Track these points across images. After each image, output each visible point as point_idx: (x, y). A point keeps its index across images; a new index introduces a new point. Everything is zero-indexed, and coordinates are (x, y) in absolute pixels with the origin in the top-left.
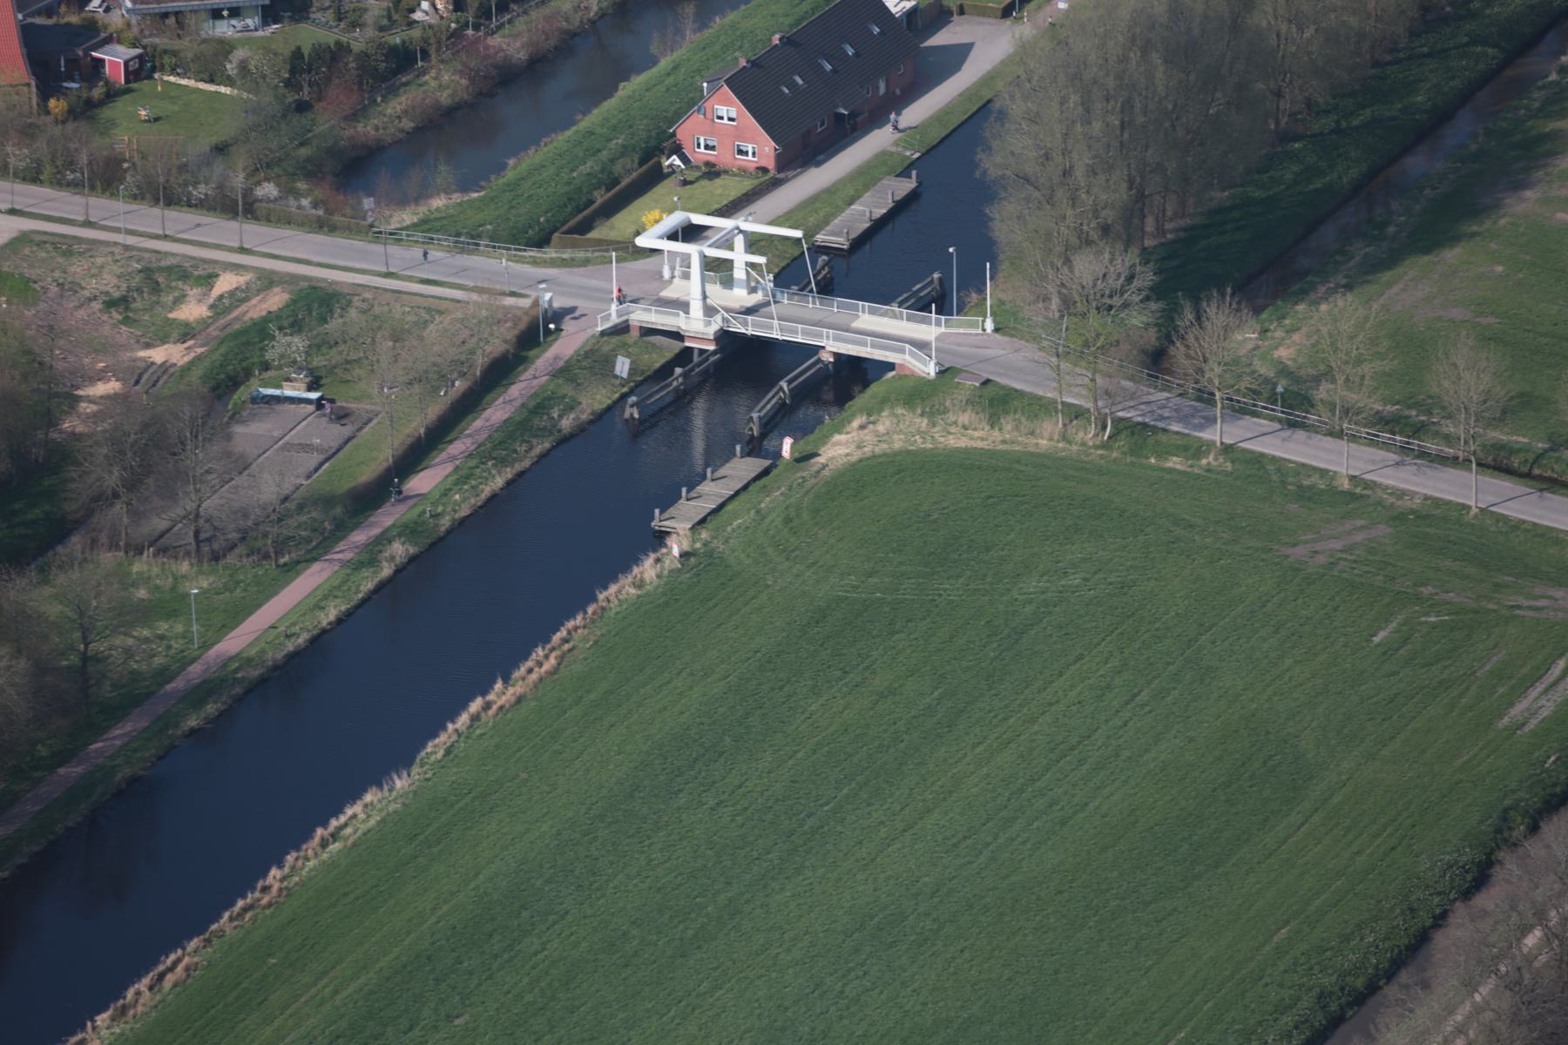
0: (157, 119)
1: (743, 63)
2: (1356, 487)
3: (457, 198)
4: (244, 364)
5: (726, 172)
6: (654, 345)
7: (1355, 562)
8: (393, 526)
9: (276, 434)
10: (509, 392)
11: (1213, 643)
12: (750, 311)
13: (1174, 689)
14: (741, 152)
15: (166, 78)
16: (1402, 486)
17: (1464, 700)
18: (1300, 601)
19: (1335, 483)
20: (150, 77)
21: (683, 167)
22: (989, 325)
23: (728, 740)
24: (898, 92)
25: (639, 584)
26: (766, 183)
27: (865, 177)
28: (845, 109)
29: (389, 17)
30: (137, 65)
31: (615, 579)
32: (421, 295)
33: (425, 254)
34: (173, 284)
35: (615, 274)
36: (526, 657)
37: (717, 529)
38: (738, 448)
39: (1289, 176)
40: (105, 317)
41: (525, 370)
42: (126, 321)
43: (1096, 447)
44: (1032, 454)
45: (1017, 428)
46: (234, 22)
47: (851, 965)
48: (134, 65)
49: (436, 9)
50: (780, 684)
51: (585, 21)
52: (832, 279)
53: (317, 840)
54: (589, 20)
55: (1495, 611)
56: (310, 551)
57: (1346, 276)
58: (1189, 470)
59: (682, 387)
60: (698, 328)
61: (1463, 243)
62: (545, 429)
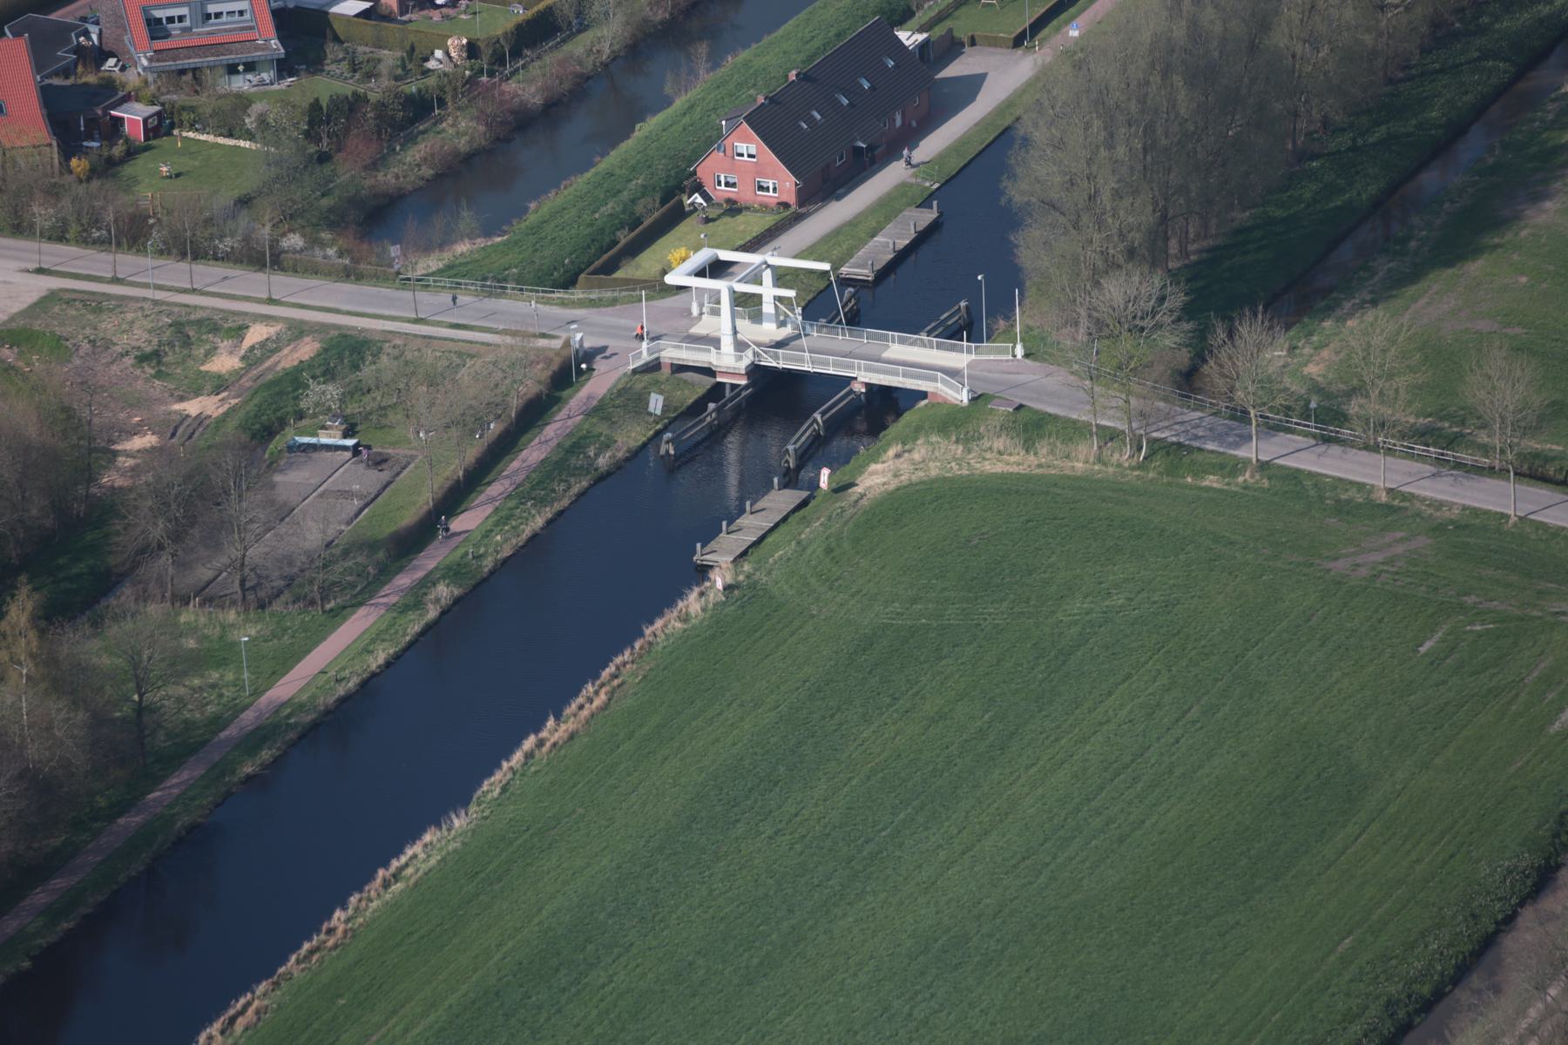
0: (178, 175)
1: (761, 100)
2: (1394, 499)
3: (481, 242)
4: (278, 414)
5: (747, 208)
6: (685, 382)
7: (1397, 573)
8: (436, 568)
9: (313, 481)
10: (545, 432)
11: (1261, 658)
12: (780, 345)
13: (1224, 704)
14: (761, 188)
15: (184, 134)
16: (1439, 497)
17: (1514, 707)
18: (1344, 614)
19: (1373, 496)
20: (169, 134)
21: (705, 204)
22: (1019, 351)
23: (782, 769)
24: (914, 124)
25: (685, 618)
26: (786, 219)
27: (886, 209)
28: (864, 142)
29: (404, 67)
30: (156, 122)
31: (661, 614)
32: (452, 340)
33: (454, 299)
34: (204, 337)
35: (646, 312)
36: (576, 694)
37: (759, 561)
38: (776, 480)
39: (1308, 195)
40: (138, 372)
41: (560, 410)
42: (159, 375)
43: (1132, 468)
44: (1069, 477)
45: (1052, 452)
46: (249, 76)
47: (918, 987)
48: (153, 122)
49: (450, 57)
50: (831, 712)
51: (598, 64)
52: (858, 311)
53: (379, 881)
54: (602, 63)
55: (1540, 618)
56: (355, 596)
57: (1371, 292)
58: (1226, 487)
59: (716, 422)
60: (729, 363)
61: (1486, 255)
62: (582, 467)
